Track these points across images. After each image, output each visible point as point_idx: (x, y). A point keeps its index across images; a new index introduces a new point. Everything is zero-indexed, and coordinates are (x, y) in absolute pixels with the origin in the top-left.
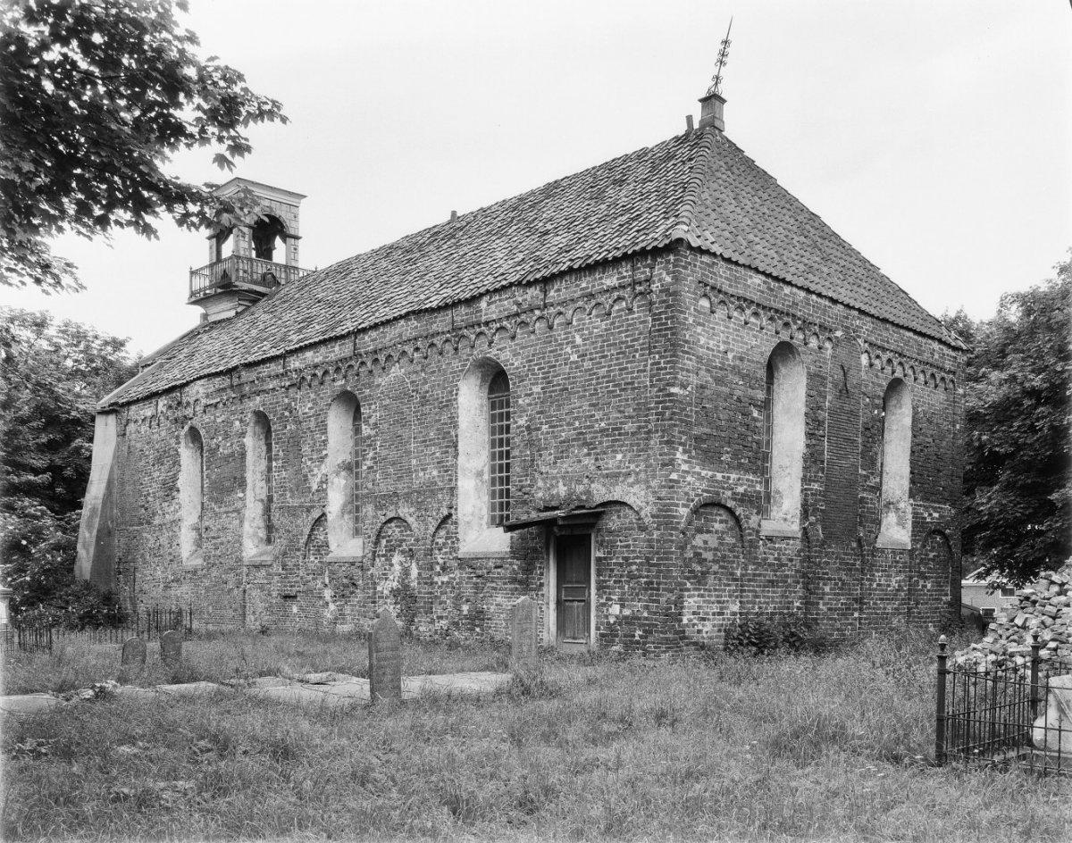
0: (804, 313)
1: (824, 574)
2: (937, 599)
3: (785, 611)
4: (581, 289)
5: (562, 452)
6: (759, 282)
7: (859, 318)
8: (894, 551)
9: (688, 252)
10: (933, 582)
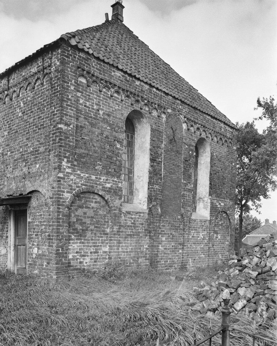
0: (148, 97)
1: (161, 231)
2: (224, 243)
3: (139, 250)
4: (23, 76)
5: (15, 166)
6: (120, 75)
7: (181, 105)
8: (201, 221)
9: (70, 48)
10: (221, 235)
